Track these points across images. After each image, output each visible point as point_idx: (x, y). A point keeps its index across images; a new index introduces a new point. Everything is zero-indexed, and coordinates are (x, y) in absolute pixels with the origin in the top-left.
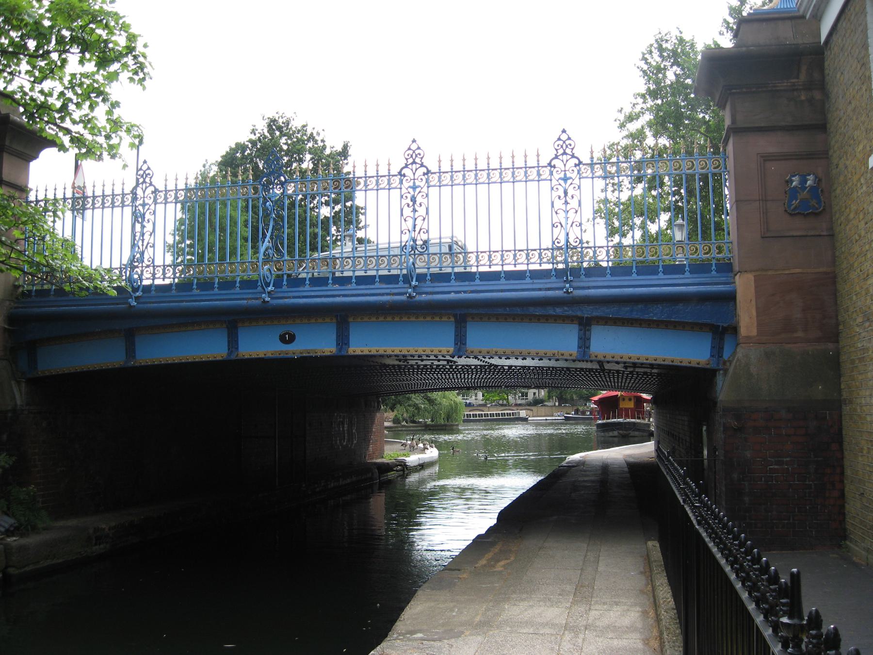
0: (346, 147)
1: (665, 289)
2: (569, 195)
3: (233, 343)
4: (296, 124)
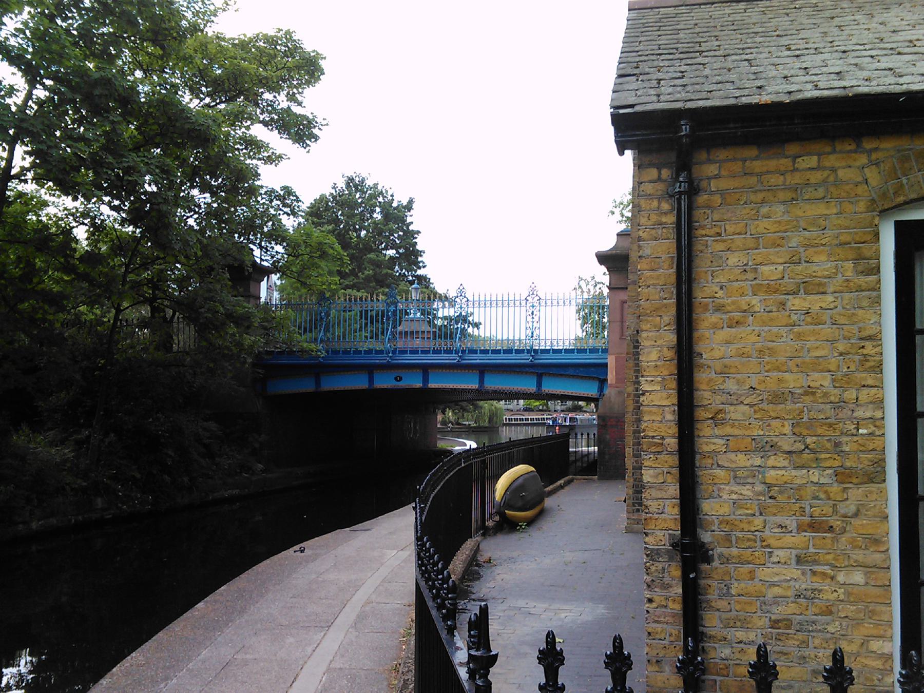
0: (411, 202)
1: (574, 361)
2: (535, 314)
3: (481, 381)
4: (369, 182)
